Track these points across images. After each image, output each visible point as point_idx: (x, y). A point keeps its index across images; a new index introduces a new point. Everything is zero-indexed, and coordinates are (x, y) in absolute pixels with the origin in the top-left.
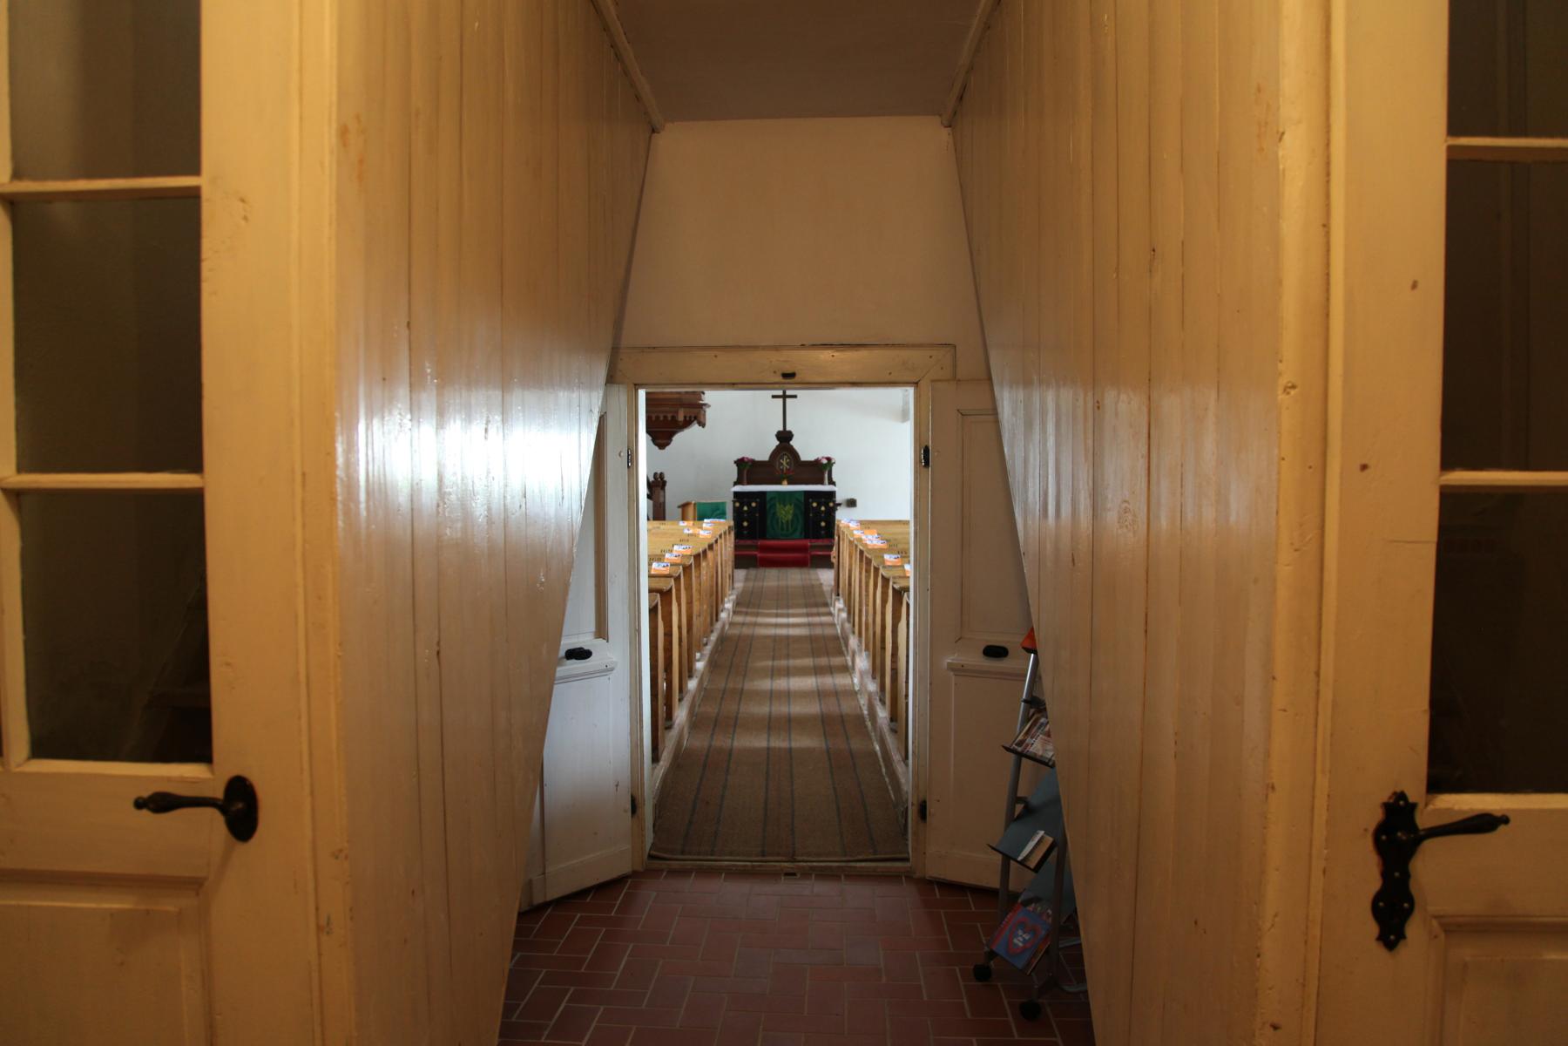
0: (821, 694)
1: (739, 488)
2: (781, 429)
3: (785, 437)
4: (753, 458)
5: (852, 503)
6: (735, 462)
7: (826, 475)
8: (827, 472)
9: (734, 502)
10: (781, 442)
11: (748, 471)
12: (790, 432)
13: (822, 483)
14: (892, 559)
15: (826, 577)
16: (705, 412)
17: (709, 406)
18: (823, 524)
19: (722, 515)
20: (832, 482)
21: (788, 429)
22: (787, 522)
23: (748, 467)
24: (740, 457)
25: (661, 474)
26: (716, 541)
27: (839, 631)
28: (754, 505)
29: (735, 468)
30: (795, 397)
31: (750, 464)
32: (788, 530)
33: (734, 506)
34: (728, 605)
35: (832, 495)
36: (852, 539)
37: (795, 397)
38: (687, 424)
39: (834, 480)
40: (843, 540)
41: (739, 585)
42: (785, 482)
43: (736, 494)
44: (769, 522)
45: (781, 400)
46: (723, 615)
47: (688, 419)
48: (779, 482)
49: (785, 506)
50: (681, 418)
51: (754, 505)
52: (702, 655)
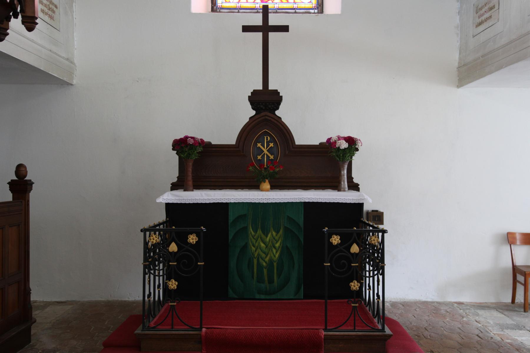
2: (260, 88)
7: (345, 172)
8: (346, 167)
10: (262, 32)
11: (196, 162)
12: (276, 93)
13: (336, 186)
19: (163, 227)
20: (354, 187)
21: (271, 87)
22: (271, 262)
23: (194, 157)
24: (180, 136)
28: (192, 239)
29: (174, 158)
30: (285, 29)
31: (200, 149)
32: (271, 281)
37: (285, 29)
39: (355, 181)
42: (266, 185)
43: (170, 207)
44: (233, 264)
45: (259, 36)
48: (255, 186)
49: (266, 232)
51: (192, 239)
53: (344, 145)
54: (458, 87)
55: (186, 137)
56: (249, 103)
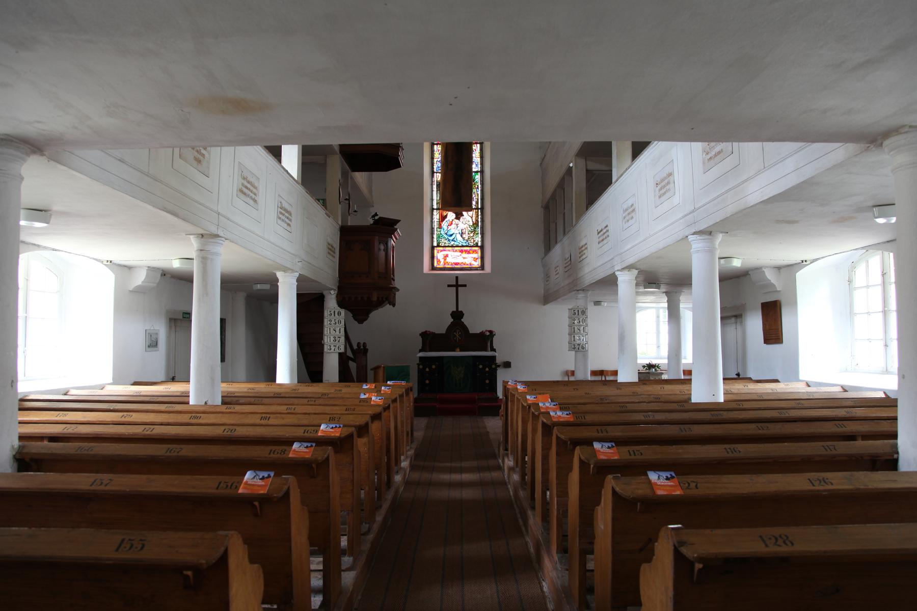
0: (482, 484)
1: (421, 354)
3: (457, 315)
4: (434, 332)
5: (507, 365)
6: (420, 335)
9: (418, 365)
12: (461, 312)
13: (486, 350)
14: (662, 481)
15: (493, 424)
16: (395, 294)
17: (398, 290)
18: (487, 381)
20: (493, 350)
21: (459, 310)
25: (364, 344)
26: (388, 408)
27: (512, 493)
29: (420, 339)
33: (419, 368)
34: (405, 464)
35: (494, 358)
36: (525, 404)
38: (380, 304)
40: (513, 401)
41: (419, 434)
43: (421, 358)
46: (398, 478)
47: (380, 299)
48: (454, 351)
50: (375, 299)
52: (407, 457)
53: (488, 334)
54: (544, 305)
55: (426, 331)
56: (297, 360)
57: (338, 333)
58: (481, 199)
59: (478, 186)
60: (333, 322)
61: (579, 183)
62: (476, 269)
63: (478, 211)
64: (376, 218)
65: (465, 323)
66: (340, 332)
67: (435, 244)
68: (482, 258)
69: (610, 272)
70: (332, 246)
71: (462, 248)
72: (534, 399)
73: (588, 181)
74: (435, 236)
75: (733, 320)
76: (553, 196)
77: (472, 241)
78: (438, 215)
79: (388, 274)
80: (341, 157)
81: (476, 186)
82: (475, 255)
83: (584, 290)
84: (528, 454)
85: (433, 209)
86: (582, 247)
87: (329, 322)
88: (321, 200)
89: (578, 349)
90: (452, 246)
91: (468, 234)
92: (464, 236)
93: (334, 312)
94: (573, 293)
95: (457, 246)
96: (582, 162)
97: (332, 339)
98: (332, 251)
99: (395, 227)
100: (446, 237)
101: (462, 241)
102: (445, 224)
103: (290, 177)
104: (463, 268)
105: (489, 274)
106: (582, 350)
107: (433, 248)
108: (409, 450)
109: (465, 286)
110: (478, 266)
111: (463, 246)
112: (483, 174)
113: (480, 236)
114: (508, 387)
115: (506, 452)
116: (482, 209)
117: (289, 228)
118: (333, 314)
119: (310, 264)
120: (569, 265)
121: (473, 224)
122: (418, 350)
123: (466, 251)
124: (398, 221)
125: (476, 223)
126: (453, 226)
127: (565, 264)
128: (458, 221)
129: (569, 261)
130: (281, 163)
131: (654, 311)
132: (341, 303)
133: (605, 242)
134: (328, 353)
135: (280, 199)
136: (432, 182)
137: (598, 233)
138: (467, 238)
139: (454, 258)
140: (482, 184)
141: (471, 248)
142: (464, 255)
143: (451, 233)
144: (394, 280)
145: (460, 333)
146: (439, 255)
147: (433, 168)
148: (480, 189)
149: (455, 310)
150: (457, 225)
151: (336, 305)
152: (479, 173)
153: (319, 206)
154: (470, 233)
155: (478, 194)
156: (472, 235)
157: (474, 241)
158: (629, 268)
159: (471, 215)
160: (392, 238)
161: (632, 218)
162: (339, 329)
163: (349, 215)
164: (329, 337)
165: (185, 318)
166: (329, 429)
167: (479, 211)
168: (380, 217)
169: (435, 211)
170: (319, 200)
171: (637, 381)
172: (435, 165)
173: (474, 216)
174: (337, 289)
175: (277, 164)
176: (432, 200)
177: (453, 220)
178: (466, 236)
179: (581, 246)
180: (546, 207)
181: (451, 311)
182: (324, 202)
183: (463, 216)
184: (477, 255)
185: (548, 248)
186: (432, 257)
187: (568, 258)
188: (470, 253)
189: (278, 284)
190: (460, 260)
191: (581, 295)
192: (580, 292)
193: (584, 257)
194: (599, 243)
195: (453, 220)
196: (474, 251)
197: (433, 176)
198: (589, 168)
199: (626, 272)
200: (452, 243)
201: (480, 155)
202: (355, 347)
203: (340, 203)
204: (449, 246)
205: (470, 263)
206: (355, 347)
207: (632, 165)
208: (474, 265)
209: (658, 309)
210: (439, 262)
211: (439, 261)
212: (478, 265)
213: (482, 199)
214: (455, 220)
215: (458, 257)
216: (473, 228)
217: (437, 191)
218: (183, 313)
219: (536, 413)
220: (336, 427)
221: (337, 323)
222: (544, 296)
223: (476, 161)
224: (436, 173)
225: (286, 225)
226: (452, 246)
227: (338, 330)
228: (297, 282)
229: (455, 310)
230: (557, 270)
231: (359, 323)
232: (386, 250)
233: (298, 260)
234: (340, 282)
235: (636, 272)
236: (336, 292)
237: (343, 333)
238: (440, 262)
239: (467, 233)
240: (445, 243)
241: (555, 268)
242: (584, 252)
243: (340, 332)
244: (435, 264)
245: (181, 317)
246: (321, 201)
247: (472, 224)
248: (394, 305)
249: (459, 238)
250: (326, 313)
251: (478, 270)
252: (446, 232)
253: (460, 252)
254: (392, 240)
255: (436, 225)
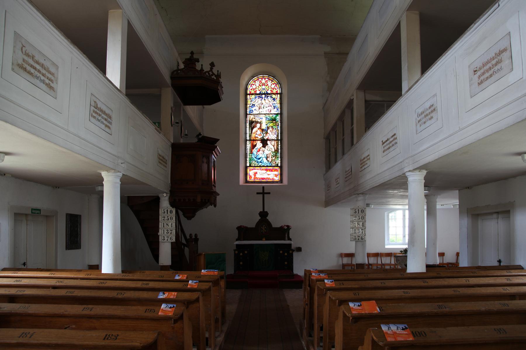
1: (237, 243)
3: (264, 214)
4: (246, 226)
5: (299, 249)
9: (235, 250)
12: (267, 212)
13: (284, 240)
17: (218, 195)
18: (286, 263)
21: (265, 210)
25: (196, 235)
29: (237, 231)
33: (235, 253)
35: (290, 245)
36: (350, 315)
38: (204, 204)
43: (237, 245)
48: (261, 240)
50: (199, 200)
55: (241, 226)
57: (170, 227)
58: (280, 133)
59: (278, 124)
60: (166, 218)
61: (359, 109)
62: (277, 182)
63: (278, 142)
64: (200, 137)
65: (269, 220)
66: (172, 226)
67: (248, 165)
68: (281, 174)
69: (400, 173)
70: (163, 158)
71: (267, 168)
72: (318, 276)
73: (366, 108)
74: (248, 159)
75: (495, 216)
76: (334, 129)
77: (274, 163)
78: (250, 144)
79: (209, 183)
80: (173, 90)
81: (277, 124)
82: (276, 173)
83: (363, 194)
84: (336, 345)
85: (247, 140)
86: (364, 159)
87: (163, 219)
88: (157, 123)
89: (359, 240)
90: (260, 166)
91: (272, 158)
92: (268, 159)
93: (167, 210)
94: (354, 196)
95: (264, 166)
96: (361, 94)
97: (166, 232)
98: (164, 162)
99: (215, 145)
100: (256, 160)
101: (267, 162)
102: (255, 151)
103: (109, 83)
104: (268, 181)
105: (286, 185)
106: (362, 240)
107: (246, 167)
108: (219, 336)
109: (269, 193)
110: (278, 180)
111: (267, 166)
112: (282, 116)
113: (280, 159)
114: (312, 278)
115: (310, 338)
116: (281, 140)
117: (107, 129)
118: (166, 212)
119: (137, 167)
120: (350, 175)
121: (275, 151)
122: (235, 240)
123: (270, 170)
124: (217, 140)
125: (277, 150)
126: (261, 152)
127: (346, 175)
128: (264, 148)
129: (349, 172)
130: (105, 74)
131: (401, 212)
132: (172, 204)
133: (391, 149)
134: (163, 242)
135: (93, 98)
136: (246, 121)
137: (383, 143)
138: (270, 161)
139: (262, 174)
140: (281, 122)
141: (273, 168)
142: (269, 172)
143: (259, 157)
144: (215, 187)
145: (266, 227)
146: (251, 173)
147: (246, 111)
148: (279, 126)
149: (262, 211)
150: (264, 151)
151: (169, 205)
152: (279, 115)
153: (148, 121)
154: (272, 157)
155: (278, 130)
156: (274, 158)
157: (275, 163)
158: (420, 168)
159: (273, 145)
160: (213, 153)
161: (432, 118)
162: (171, 223)
163: (182, 138)
164: (163, 230)
165: (33, 213)
166: (205, 272)
167: (279, 141)
168: (203, 136)
169: (248, 141)
170: (155, 123)
171: (425, 272)
172: (248, 109)
173: (275, 145)
174: (169, 193)
175: (102, 76)
176: (246, 133)
177: (260, 148)
178: (270, 159)
179: (363, 158)
180: (328, 138)
181: (259, 211)
182: (158, 124)
183: (268, 145)
184: (278, 172)
185: (329, 166)
186: (246, 174)
187: (349, 170)
188: (273, 171)
189: (104, 182)
190: (265, 176)
191: (361, 198)
192: (360, 195)
193: (366, 166)
194: (384, 152)
195: (260, 148)
196: (275, 170)
197: (246, 117)
198: (367, 99)
199: (417, 173)
200: (260, 164)
201: (280, 102)
202: (188, 237)
203: (172, 126)
204: (257, 166)
205: (273, 178)
206: (188, 237)
207: (422, 77)
208: (275, 179)
209: (404, 210)
210: (250, 178)
211: (250, 177)
212: (278, 179)
213: (281, 133)
214: (262, 148)
215: (264, 174)
216: (274, 154)
217: (249, 127)
218: (32, 209)
219: (381, 344)
220: (208, 271)
221: (170, 219)
222: (325, 202)
223: (277, 107)
224: (249, 114)
225: (104, 126)
226: (260, 166)
227: (170, 224)
228: (120, 181)
229: (262, 211)
230: (338, 181)
231: (188, 220)
232: (208, 163)
233: (120, 161)
234: (171, 187)
235: (424, 172)
236: (169, 195)
237: (175, 227)
238: (252, 178)
239: (270, 157)
240: (255, 164)
241: (336, 180)
242: (367, 162)
243: (172, 226)
244: (248, 179)
245: (30, 213)
246: (157, 124)
247: (274, 151)
248: (215, 206)
249: (265, 160)
250: (161, 211)
251: (278, 183)
252: (256, 156)
253: (266, 170)
254: (213, 155)
255: (248, 152)
